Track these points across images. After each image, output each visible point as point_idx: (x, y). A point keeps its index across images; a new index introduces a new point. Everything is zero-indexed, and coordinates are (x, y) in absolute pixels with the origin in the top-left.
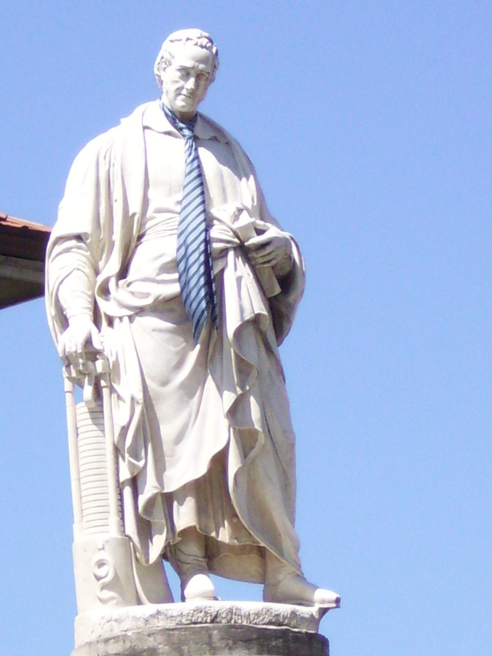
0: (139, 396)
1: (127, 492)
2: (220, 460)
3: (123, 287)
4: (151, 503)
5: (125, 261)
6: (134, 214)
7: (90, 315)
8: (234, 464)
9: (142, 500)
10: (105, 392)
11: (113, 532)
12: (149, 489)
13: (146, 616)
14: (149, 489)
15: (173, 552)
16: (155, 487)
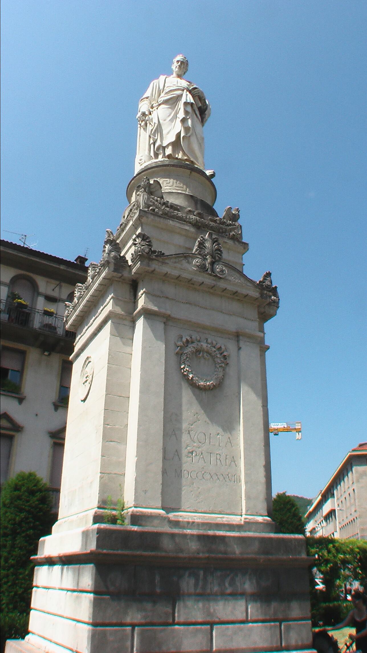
0: (157, 122)
1: (152, 146)
2: (178, 135)
4: (158, 148)
6: (161, 89)
8: (182, 134)
9: (157, 145)
10: (148, 124)
12: (158, 143)
13: (182, 276)
14: (158, 143)
15: (157, 130)
16: (159, 143)
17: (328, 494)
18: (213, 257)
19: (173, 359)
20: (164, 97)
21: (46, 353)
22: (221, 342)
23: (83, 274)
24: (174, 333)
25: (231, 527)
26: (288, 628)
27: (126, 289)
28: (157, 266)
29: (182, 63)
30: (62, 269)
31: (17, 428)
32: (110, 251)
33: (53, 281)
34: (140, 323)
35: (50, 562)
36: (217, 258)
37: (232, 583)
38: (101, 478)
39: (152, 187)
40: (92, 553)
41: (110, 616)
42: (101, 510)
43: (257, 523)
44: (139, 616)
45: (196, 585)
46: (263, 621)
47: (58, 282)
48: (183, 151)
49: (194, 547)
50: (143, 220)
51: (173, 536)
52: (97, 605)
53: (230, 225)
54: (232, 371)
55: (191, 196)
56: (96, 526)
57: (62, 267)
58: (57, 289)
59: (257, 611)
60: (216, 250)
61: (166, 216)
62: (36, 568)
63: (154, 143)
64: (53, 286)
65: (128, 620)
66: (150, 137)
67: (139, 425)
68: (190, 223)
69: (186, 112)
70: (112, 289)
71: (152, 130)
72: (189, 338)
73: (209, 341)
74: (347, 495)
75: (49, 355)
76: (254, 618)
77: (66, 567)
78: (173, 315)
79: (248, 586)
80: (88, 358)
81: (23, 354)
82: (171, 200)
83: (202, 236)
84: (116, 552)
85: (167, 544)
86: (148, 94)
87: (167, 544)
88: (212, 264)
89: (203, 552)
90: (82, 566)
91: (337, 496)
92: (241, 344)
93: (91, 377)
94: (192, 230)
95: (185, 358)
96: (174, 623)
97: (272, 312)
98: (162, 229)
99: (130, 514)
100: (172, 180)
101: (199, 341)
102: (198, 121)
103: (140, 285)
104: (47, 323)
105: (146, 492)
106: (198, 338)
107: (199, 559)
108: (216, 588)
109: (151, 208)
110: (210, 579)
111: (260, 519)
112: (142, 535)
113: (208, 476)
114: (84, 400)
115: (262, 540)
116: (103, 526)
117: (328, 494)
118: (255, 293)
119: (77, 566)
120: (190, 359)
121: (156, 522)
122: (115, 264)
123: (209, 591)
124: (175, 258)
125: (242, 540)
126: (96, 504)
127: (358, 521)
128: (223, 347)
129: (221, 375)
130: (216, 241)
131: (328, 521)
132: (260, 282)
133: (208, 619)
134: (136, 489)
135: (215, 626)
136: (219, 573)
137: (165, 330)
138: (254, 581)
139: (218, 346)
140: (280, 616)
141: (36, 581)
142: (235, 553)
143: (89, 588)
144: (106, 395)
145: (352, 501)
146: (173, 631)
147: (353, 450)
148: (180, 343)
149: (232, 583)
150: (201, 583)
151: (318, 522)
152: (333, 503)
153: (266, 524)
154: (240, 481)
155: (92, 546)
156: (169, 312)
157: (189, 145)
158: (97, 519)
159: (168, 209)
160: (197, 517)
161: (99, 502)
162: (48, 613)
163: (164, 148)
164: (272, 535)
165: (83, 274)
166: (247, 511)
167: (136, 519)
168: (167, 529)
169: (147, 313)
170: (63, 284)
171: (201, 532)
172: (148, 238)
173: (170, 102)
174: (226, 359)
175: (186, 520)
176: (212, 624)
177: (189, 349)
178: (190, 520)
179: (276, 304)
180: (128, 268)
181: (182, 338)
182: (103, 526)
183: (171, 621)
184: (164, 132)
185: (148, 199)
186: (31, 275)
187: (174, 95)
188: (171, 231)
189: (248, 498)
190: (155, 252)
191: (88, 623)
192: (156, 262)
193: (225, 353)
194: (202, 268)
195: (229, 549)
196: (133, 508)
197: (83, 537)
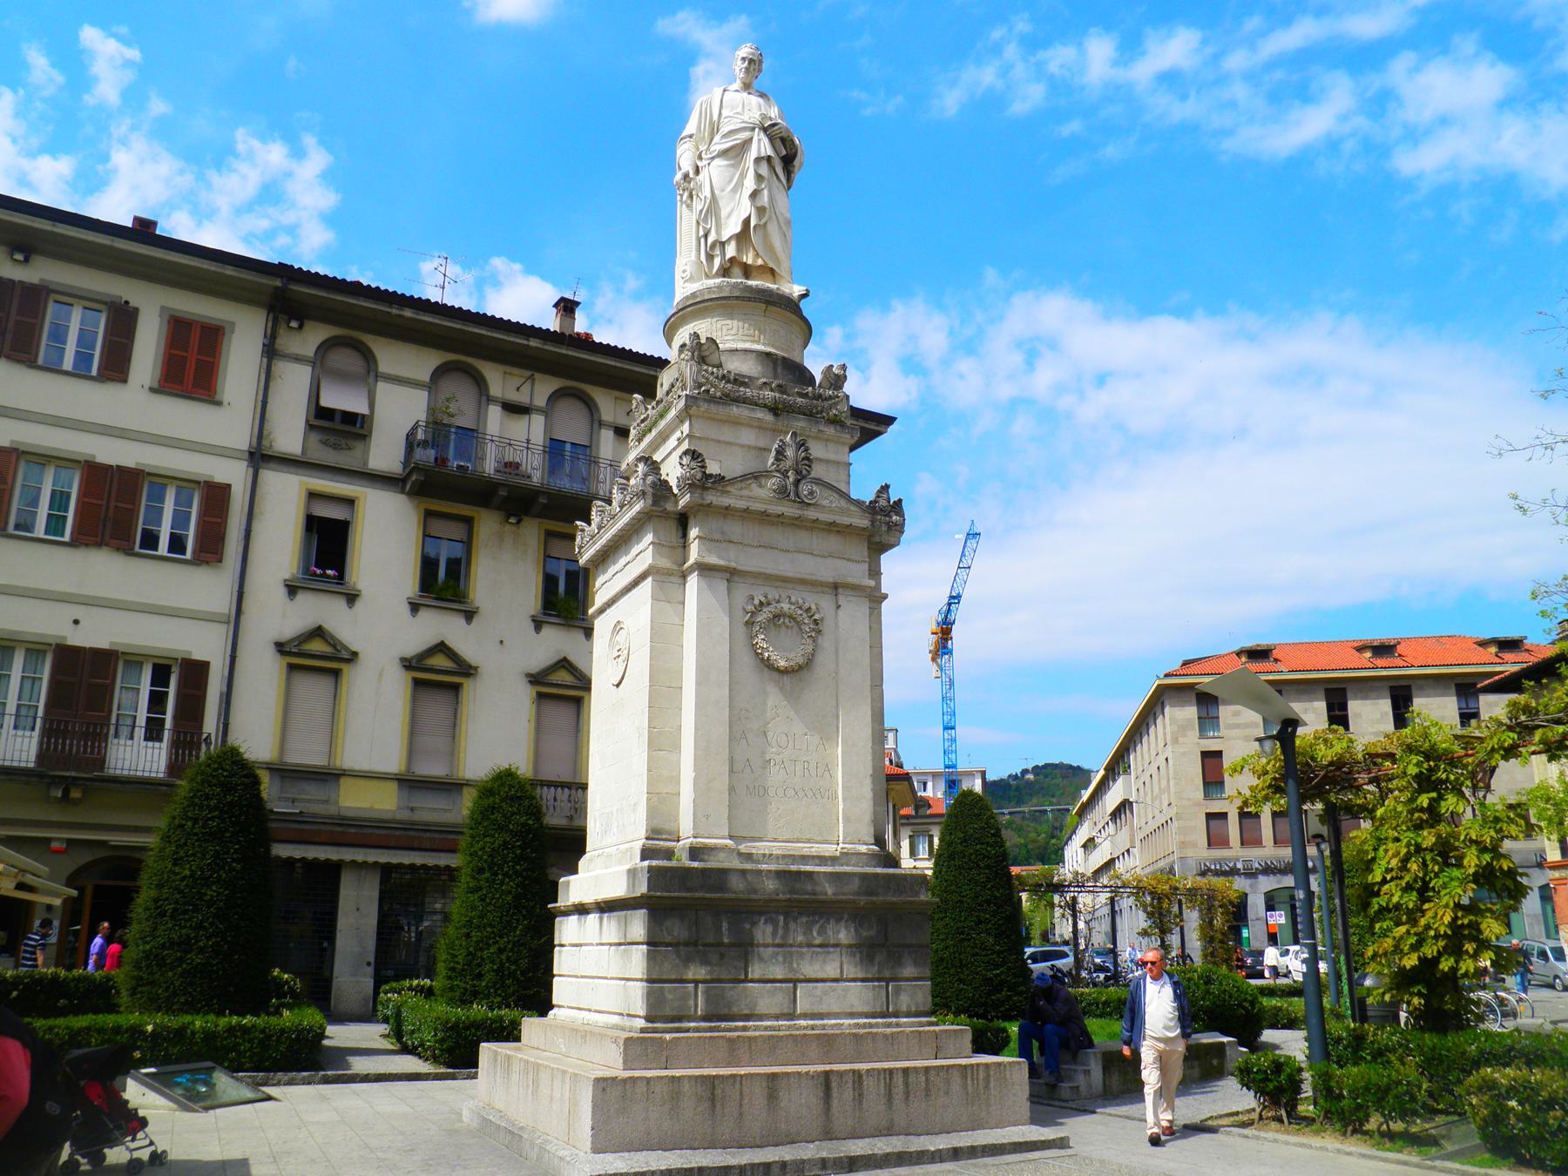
0: (709, 195)
1: (702, 240)
2: (747, 222)
3: (1530, 882)
4: (713, 246)
5: (823, 529)
7: (1416, 69)
8: (753, 223)
9: (710, 241)
10: (695, 197)
11: (693, 257)
17: (1118, 764)
18: (798, 472)
19: (741, 631)
20: (719, 145)
21: (512, 520)
22: (811, 600)
24: (742, 591)
25: (822, 860)
26: (897, 991)
27: (672, 530)
28: (715, 498)
29: (751, 61)
30: (531, 347)
31: (467, 670)
32: (646, 475)
33: (516, 371)
34: (693, 581)
35: (582, 910)
36: (804, 472)
37: (822, 932)
38: (649, 800)
39: (705, 347)
40: (643, 896)
41: (668, 971)
42: (651, 842)
43: (859, 854)
44: (703, 972)
45: (774, 934)
46: (863, 980)
47: (527, 373)
48: (755, 250)
50: (691, 412)
51: (744, 872)
52: (651, 957)
53: (830, 398)
54: (826, 642)
55: (768, 354)
56: (646, 863)
57: (534, 343)
58: (526, 388)
60: (803, 459)
61: (729, 399)
62: (557, 920)
63: (706, 236)
64: (517, 381)
65: (690, 976)
66: (698, 223)
67: (696, 729)
68: (765, 406)
69: (759, 178)
70: (650, 527)
71: (701, 211)
72: (763, 599)
73: (793, 600)
74: (1154, 770)
75: (519, 522)
76: (851, 976)
77: (606, 915)
78: (739, 568)
79: (844, 935)
80: (618, 622)
81: (469, 522)
82: (735, 366)
83: (782, 438)
84: (672, 894)
85: (736, 883)
86: (691, 128)
87: (736, 883)
88: (797, 483)
89: (784, 893)
90: (629, 912)
91: (1136, 769)
92: (842, 600)
93: (626, 652)
94: (769, 417)
96: (746, 980)
97: (892, 540)
98: (721, 421)
99: (688, 846)
100: (735, 322)
101: (778, 602)
102: (781, 187)
103: (691, 522)
104: (511, 460)
105: (708, 817)
106: (777, 597)
107: (777, 901)
108: (800, 938)
109: (703, 389)
110: (792, 926)
111: (863, 849)
112: (704, 871)
113: (791, 792)
114: (618, 686)
115: (864, 877)
116: (654, 863)
117: (1118, 764)
118: (862, 522)
119: (623, 913)
120: (765, 629)
121: (722, 855)
122: (654, 495)
124: (741, 481)
126: (643, 833)
127: (1174, 826)
128: (813, 607)
130: (803, 444)
131: (1118, 820)
132: (871, 502)
133: (790, 976)
134: (694, 814)
135: (799, 985)
136: (804, 919)
137: (729, 590)
138: (852, 930)
139: (806, 606)
140: (887, 974)
141: (560, 931)
142: (826, 894)
143: (641, 939)
144: (650, 686)
145: (1164, 783)
146: (745, 989)
147: (1167, 675)
148: (750, 608)
149: (822, 932)
150: (780, 932)
151: (1100, 826)
152: (1128, 786)
153: (872, 855)
154: (837, 798)
155: (643, 889)
156: (733, 565)
157: (766, 237)
158: (646, 854)
159: (729, 386)
160: (777, 848)
161: (647, 831)
162: (582, 977)
163: (723, 244)
164: (879, 870)
166: (844, 838)
167: (695, 852)
168: (736, 864)
169: (704, 569)
170: (537, 375)
171: (781, 867)
172: (700, 455)
173: (731, 154)
174: (817, 624)
175: (762, 852)
176: (795, 982)
177: (761, 617)
178: (767, 852)
179: (899, 528)
180: (673, 498)
181: (753, 599)
182: (654, 863)
183: (743, 977)
184: (724, 213)
185: (699, 372)
186: (471, 360)
187: (738, 142)
188: (736, 423)
189: (847, 820)
190: (711, 476)
191: (641, 980)
192: (713, 492)
193: (816, 617)
194: (782, 492)
195: (818, 889)
196: (692, 839)
197: (628, 877)
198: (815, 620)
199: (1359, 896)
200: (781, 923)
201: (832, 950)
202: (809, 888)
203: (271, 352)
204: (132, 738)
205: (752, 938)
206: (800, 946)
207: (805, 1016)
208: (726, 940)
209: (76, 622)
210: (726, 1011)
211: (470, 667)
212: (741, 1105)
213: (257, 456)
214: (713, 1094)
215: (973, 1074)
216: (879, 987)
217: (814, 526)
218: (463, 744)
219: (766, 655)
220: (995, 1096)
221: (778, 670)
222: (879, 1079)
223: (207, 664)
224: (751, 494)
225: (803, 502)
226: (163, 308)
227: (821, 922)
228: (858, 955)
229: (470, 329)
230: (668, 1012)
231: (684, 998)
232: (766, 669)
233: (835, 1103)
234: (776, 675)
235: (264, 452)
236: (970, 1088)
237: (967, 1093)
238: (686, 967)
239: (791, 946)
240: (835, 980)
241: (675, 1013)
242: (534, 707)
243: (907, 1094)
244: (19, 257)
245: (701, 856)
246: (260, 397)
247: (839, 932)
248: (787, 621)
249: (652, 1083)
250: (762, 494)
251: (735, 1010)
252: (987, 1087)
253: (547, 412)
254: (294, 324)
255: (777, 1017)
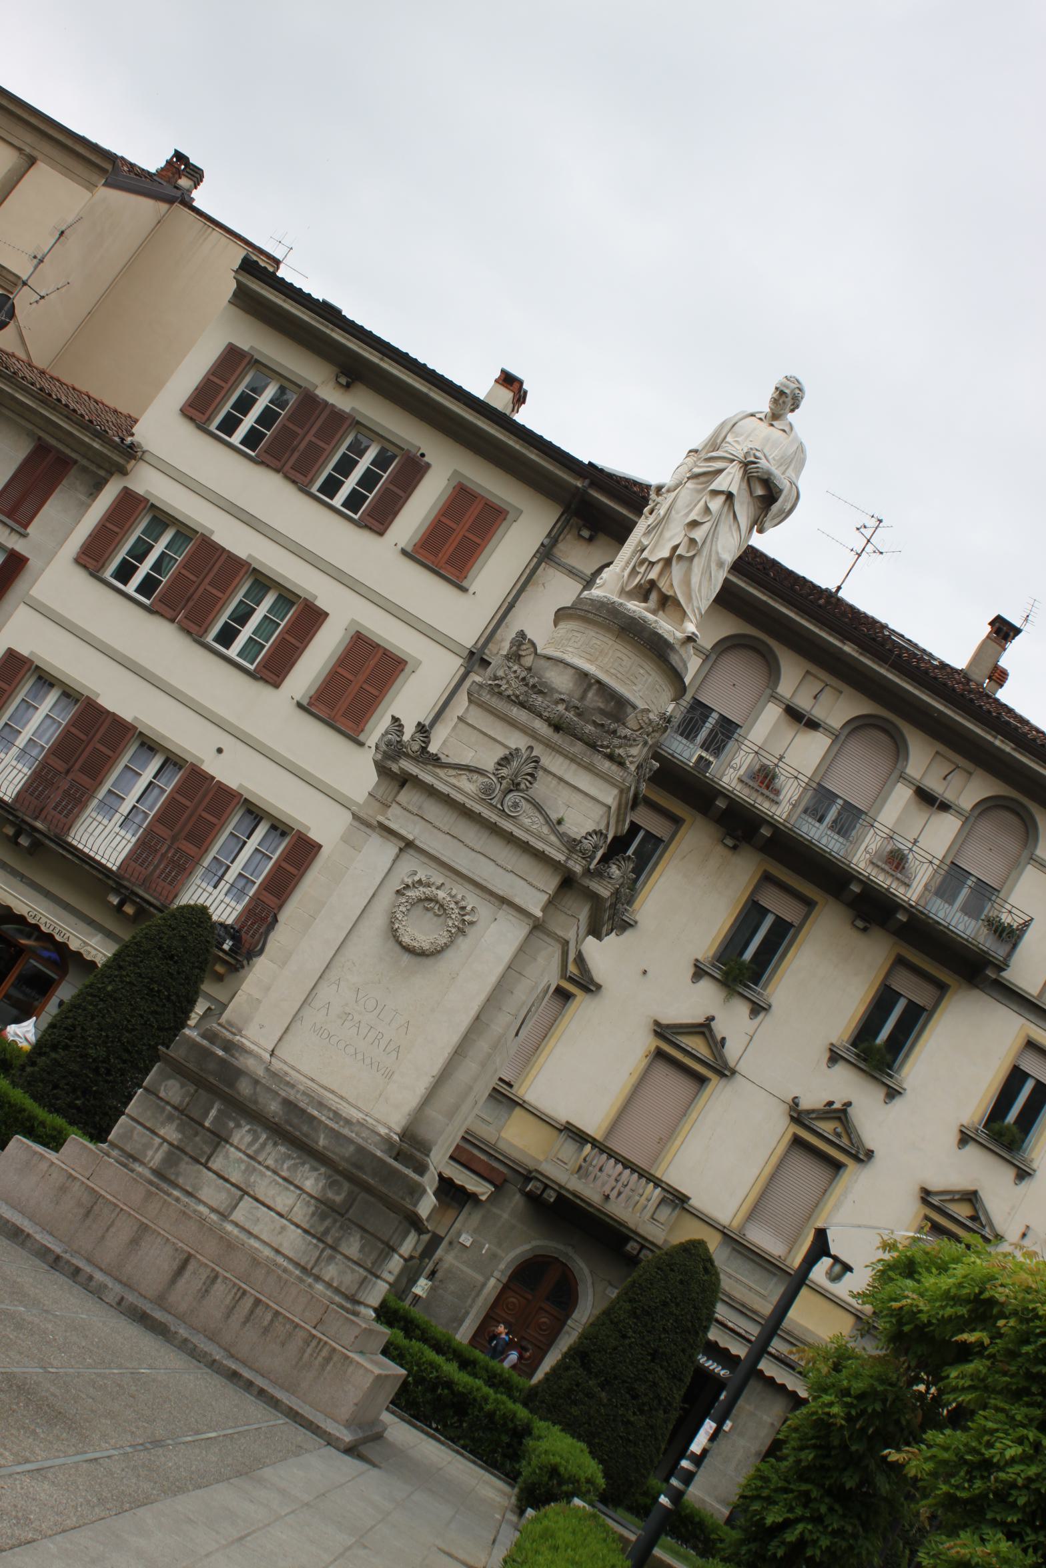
2: (676, 548)
9: (644, 556)
22: (472, 900)
23: (631, 516)
45: (250, 1144)
46: (306, 1231)
49: (272, 1108)
54: (463, 944)
59: (305, 1216)
65: (162, 1132)
76: (295, 1220)
78: (417, 843)
95: (404, 900)
113: (351, 1050)
123: (260, 1159)
125: (336, 1135)
128: (469, 908)
129: (442, 941)
133: (243, 1186)
138: (321, 1185)
139: (463, 904)
142: (317, 1143)
148: (409, 881)
150: (257, 1146)
165: (631, 516)
198: (464, 920)
199: (772, 1425)
200: (261, 1140)
201: (292, 1188)
202: (305, 1128)
203: (546, 554)
204: (215, 887)
205: (230, 1136)
206: (267, 1168)
207: (236, 1225)
208: (207, 1124)
209: (220, 751)
210: (173, 1177)
211: (592, 981)
212: (108, 1229)
213: (475, 657)
214: (92, 1207)
215: (317, 1347)
216: (316, 1246)
217: (509, 839)
218: (542, 1059)
219: (396, 926)
220: (325, 1379)
221: (400, 943)
222: (230, 1291)
223: (320, 847)
224: (457, 784)
225: (503, 811)
226: (456, 472)
227: (298, 1161)
228: (312, 1209)
229: (777, 606)
230: (128, 1148)
231: (147, 1146)
232: (392, 939)
233: (182, 1282)
234: (398, 949)
235: (485, 657)
236: (306, 1355)
237: (301, 1358)
238: (163, 1124)
239: (260, 1163)
240: (281, 1215)
241: (132, 1152)
242: (645, 1062)
243: (247, 1320)
244: (343, 381)
245: (234, 1052)
246: (510, 599)
247: (307, 1178)
248: (436, 907)
249: (53, 1167)
250: (466, 788)
251: (181, 1181)
252: (323, 1367)
253: (836, 737)
254: (586, 533)
255: (213, 1210)
